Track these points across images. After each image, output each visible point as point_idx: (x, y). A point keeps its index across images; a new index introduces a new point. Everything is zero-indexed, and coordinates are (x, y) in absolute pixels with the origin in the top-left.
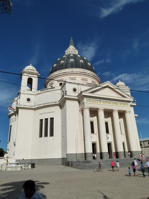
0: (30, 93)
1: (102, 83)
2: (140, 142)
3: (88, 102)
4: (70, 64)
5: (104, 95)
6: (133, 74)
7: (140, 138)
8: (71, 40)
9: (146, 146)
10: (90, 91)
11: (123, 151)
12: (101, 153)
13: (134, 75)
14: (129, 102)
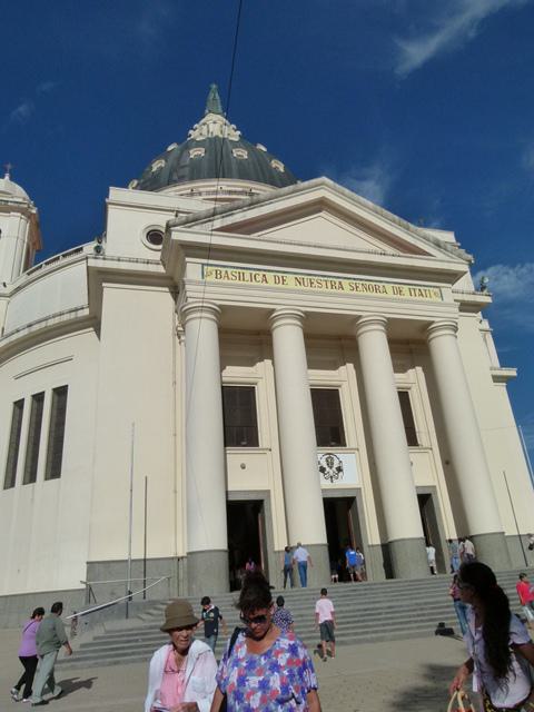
1: (291, 187)
3: (211, 279)
4: (187, 169)
5: (313, 242)
6: (528, 265)
8: (214, 95)
10: (218, 223)
11: (422, 535)
12: (387, 548)
14: (451, 277)
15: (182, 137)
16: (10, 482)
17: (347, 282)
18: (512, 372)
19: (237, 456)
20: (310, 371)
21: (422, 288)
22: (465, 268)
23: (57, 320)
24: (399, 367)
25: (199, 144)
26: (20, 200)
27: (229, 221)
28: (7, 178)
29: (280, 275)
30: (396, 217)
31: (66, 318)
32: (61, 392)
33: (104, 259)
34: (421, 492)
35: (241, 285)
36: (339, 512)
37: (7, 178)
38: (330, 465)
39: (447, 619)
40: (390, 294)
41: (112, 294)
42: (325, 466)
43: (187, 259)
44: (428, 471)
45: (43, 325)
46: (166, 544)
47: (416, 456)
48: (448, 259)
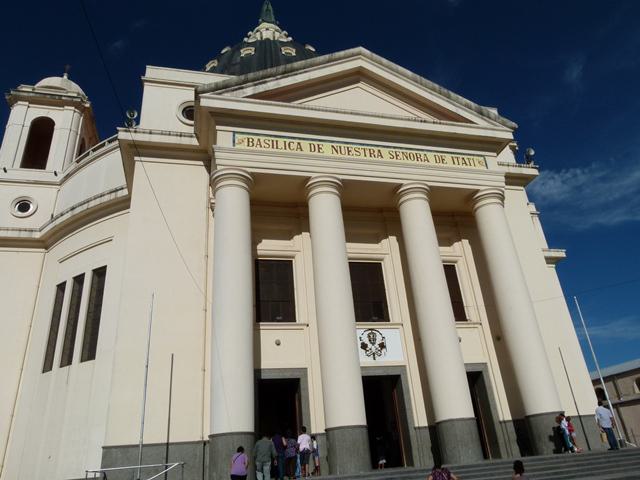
0: (32, 179)
1: (327, 56)
2: (596, 382)
5: (349, 108)
6: (572, 170)
7: (591, 367)
8: (268, 7)
9: (630, 398)
10: (250, 91)
12: (435, 429)
13: (575, 176)
14: (496, 146)
15: (237, 42)
16: (48, 366)
17: (387, 150)
18: (561, 254)
19: (270, 333)
20: (349, 245)
21: (465, 157)
22: (510, 136)
23: (98, 201)
24: (445, 240)
25: (249, 45)
26: (75, 95)
27: (261, 88)
28: (65, 77)
29: (315, 143)
30: (437, 86)
31: (106, 198)
32: (100, 273)
33: (135, 132)
34: (471, 370)
35: (275, 153)
36: (382, 391)
37: (65, 77)
38: (373, 341)
39: (552, 458)
40: (432, 162)
41: (144, 167)
42: (366, 341)
43: (218, 127)
44: (478, 348)
45: (85, 207)
46: (190, 429)
47: (463, 330)
48: (492, 126)
